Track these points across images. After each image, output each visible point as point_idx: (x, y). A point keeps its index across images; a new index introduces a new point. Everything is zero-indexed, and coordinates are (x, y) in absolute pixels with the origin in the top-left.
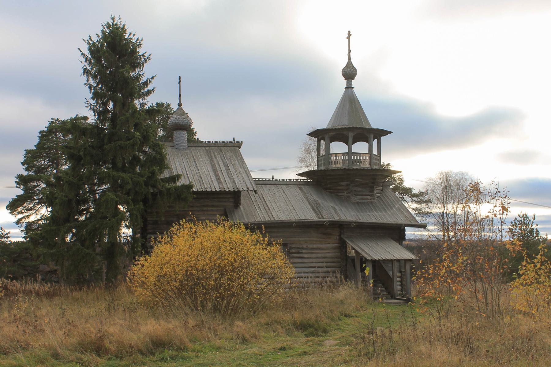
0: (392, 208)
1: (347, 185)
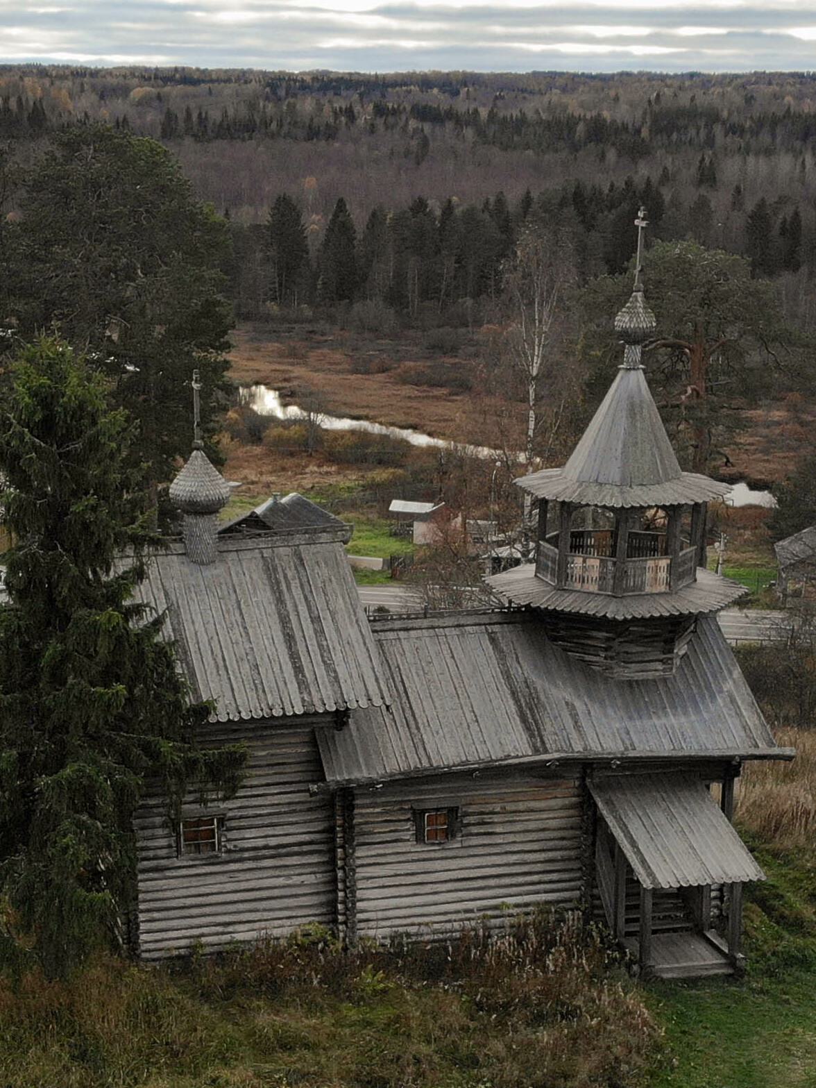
0: (713, 697)
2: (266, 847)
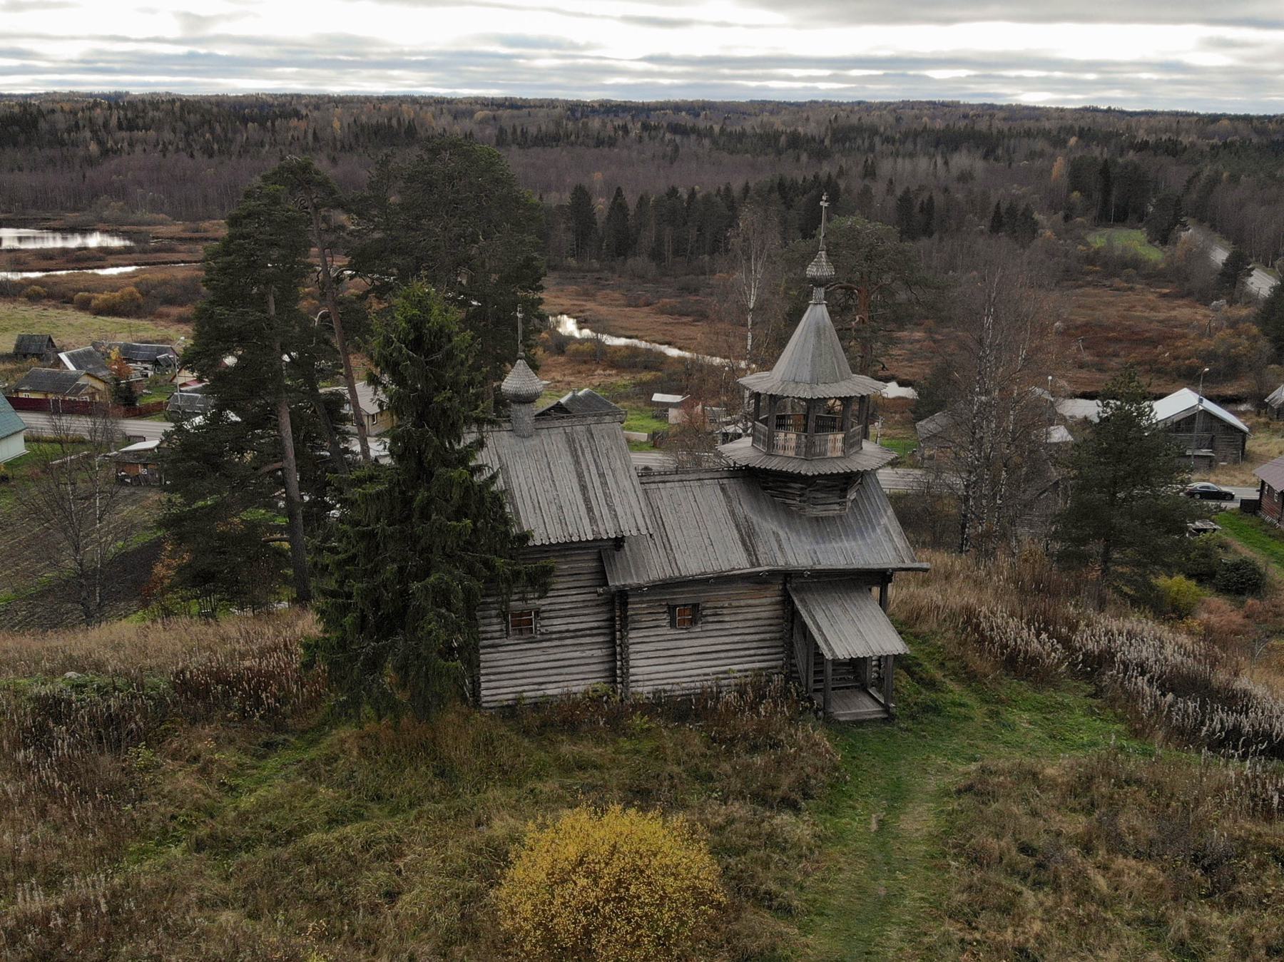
1: (802, 489)
2: (568, 631)
